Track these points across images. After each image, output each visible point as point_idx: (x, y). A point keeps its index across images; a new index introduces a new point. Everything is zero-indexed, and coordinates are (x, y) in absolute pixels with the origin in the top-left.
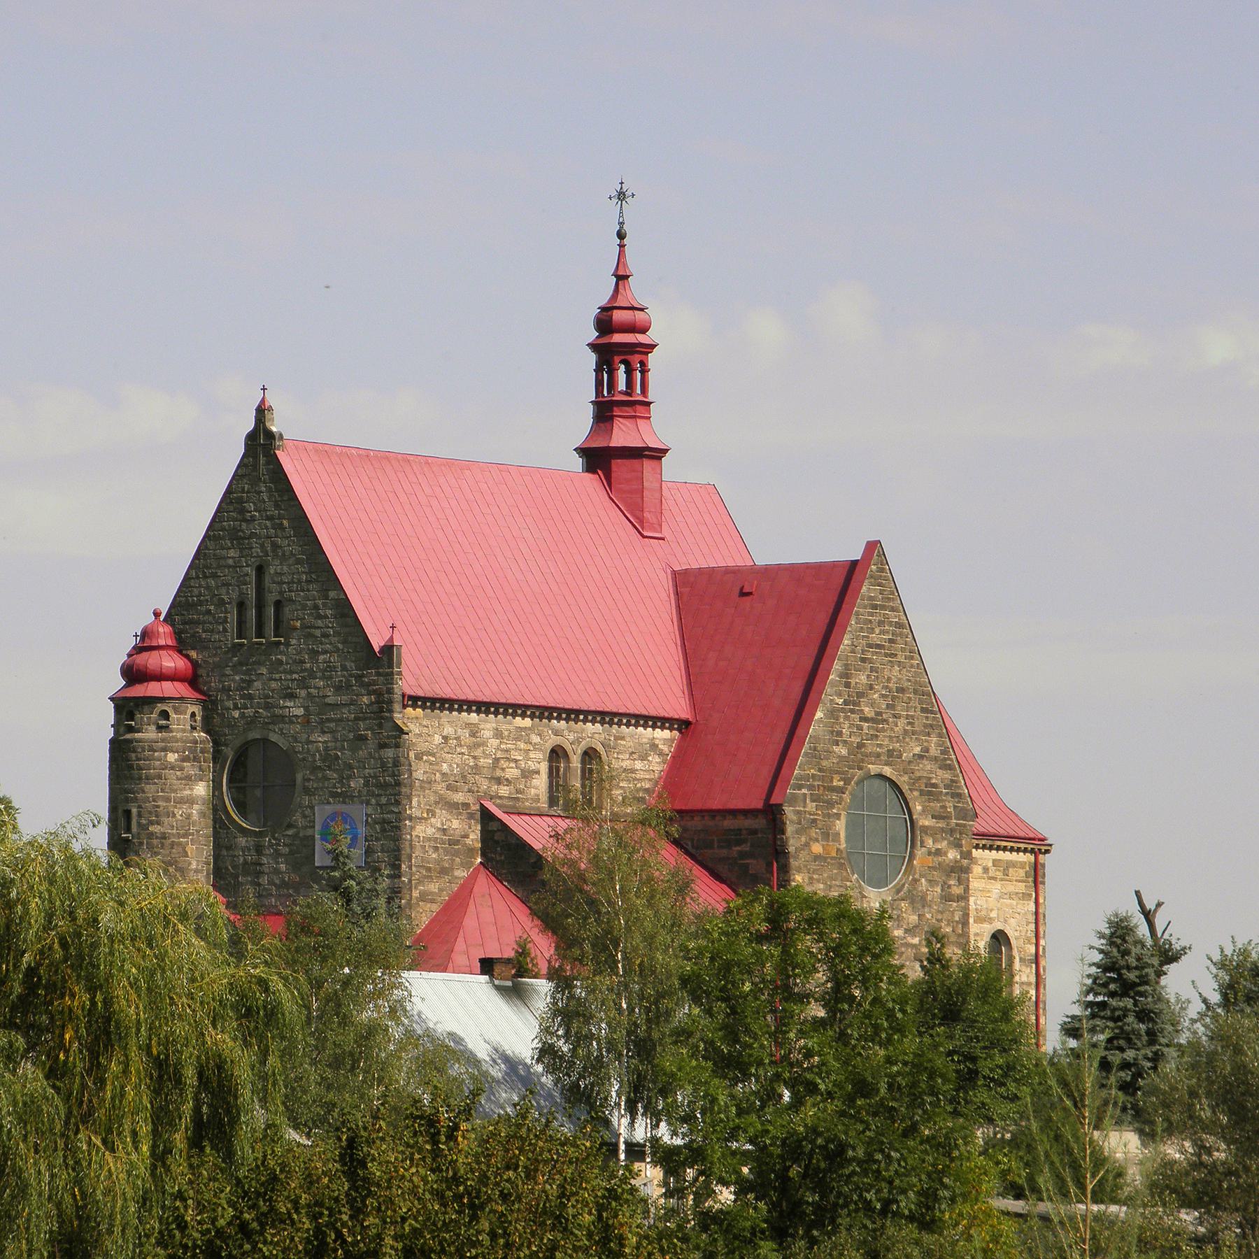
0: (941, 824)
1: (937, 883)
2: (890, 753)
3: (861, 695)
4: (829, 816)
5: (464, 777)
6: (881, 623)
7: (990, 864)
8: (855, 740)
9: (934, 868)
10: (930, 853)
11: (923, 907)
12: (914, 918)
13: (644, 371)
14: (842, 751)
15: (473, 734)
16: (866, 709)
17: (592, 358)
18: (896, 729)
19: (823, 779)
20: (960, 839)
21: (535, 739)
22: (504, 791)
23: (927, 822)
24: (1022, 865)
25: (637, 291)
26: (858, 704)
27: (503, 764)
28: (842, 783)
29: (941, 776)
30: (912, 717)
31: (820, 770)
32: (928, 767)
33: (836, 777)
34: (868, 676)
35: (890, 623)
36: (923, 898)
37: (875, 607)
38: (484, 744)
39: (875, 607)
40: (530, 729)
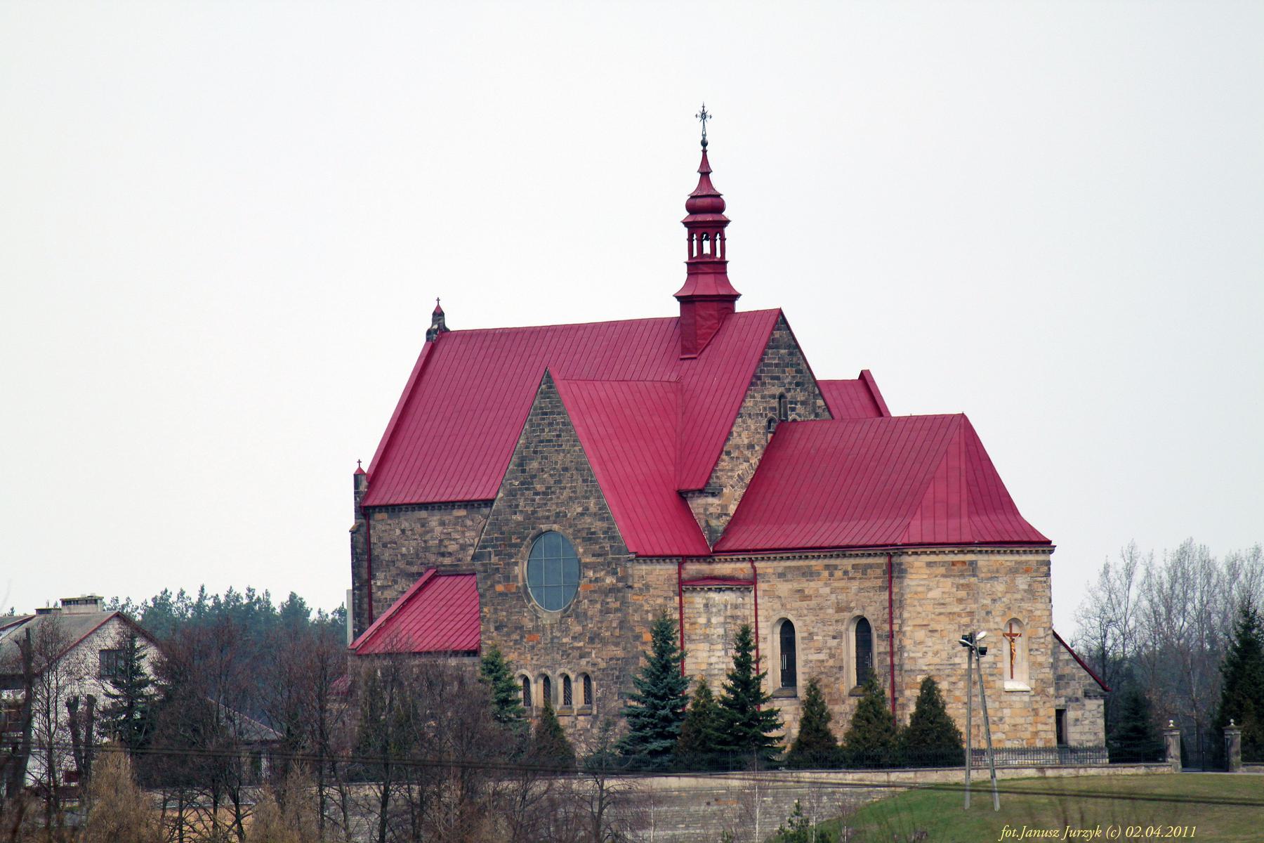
0: (600, 560)
1: (597, 602)
2: (558, 514)
3: (534, 477)
4: (508, 564)
5: (417, 555)
6: (550, 424)
7: (850, 568)
8: (529, 509)
9: (595, 592)
10: (591, 581)
11: (586, 620)
12: (578, 629)
13: (723, 240)
14: (519, 518)
15: (423, 526)
16: (538, 486)
17: (685, 231)
18: (561, 497)
19: (503, 539)
20: (616, 569)
21: (469, 523)
22: (447, 561)
23: (588, 559)
24: (879, 566)
25: (719, 182)
26: (532, 484)
27: (446, 542)
28: (519, 540)
29: (598, 526)
30: (575, 487)
31: (501, 533)
32: (589, 520)
33: (514, 537)
34: (540, 463)
35: (558, 424)
36: (585, 614)
37: (546, 414)
38: (432, 531)
39: (546, 414)
40: (465, 516)
